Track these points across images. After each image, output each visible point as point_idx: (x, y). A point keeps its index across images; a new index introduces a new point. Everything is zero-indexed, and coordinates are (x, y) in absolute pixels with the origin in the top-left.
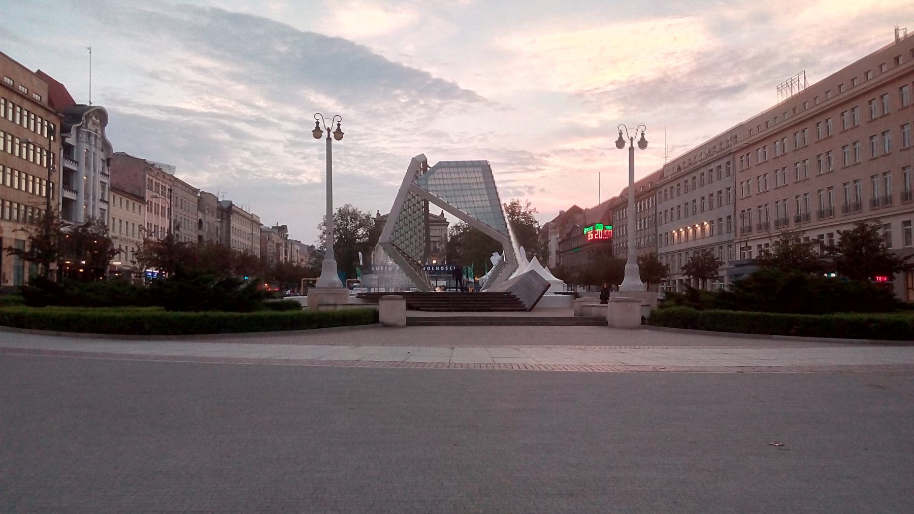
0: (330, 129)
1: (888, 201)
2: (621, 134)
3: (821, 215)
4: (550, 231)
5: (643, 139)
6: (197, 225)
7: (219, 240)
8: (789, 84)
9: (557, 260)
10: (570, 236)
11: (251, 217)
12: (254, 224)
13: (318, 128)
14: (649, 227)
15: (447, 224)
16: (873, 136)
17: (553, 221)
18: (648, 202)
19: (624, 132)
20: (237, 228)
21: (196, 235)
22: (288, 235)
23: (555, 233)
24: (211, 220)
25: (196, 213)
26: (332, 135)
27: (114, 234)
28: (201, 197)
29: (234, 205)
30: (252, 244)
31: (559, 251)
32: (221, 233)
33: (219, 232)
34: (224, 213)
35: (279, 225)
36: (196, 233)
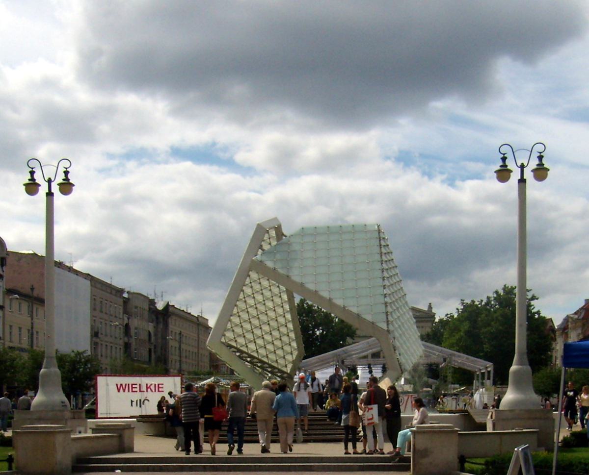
2: (504, 159)
4: (570, 326)
5: (541, 165)
6: (122, 330)
7: (152, 347)
17: (576, 313)
19: (509, 156)
23: (575, 328)
25: (121, 317)
27: (11, 345)
28: (128, 299)
30: (198, 350)
33: (153, 339)
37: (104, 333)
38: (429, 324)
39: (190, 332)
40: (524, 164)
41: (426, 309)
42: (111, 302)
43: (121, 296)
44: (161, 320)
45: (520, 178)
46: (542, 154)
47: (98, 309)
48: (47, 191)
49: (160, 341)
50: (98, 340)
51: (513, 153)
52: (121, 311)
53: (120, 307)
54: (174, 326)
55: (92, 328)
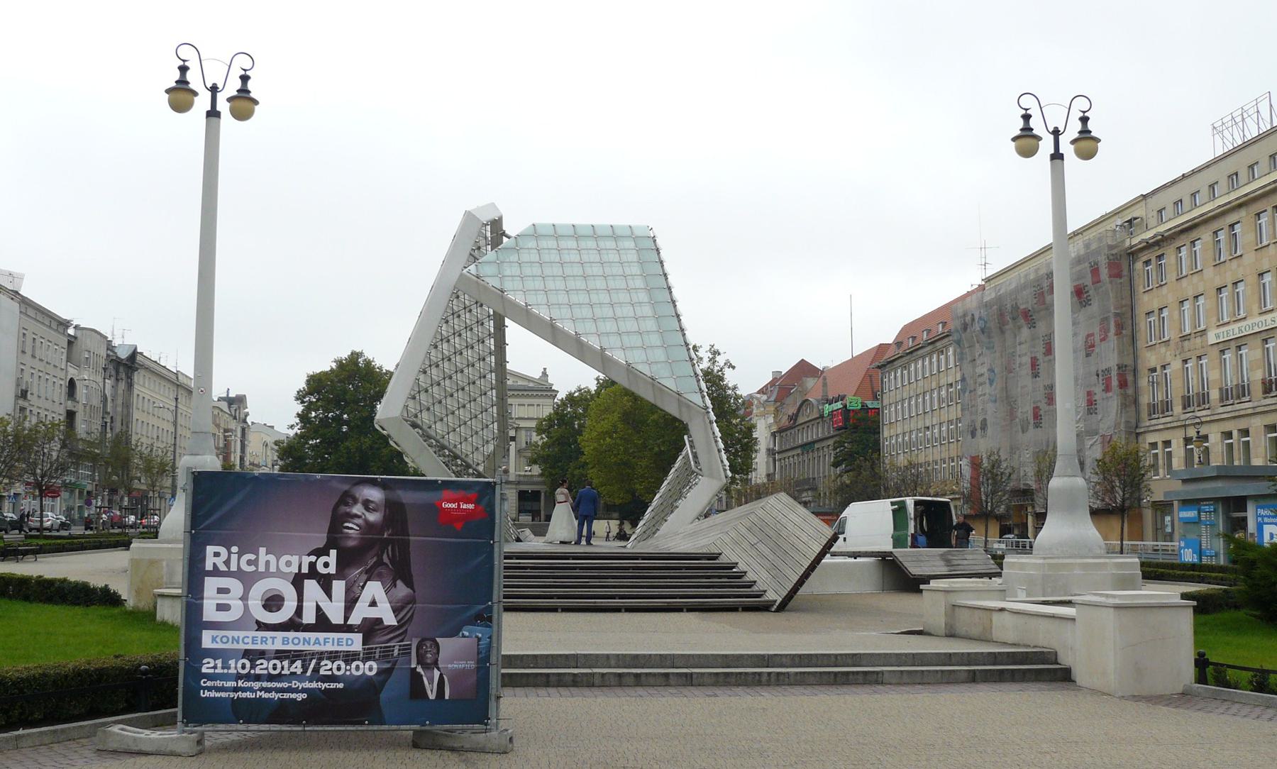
0: (221, 88)
1: (1242, 391)
3: (1225, 395)
5: (244, 91)
6: (65, 390)
8: (1239, 119)
9: (768, 468)
10: (796, 420)
11: (174, 377)
12: (181, 391)
13: (183, 81)
14: (940, 408)
15: (554, 394)
16: (1264, 273)
17: (761, 391)
18: (931, 363)
20: (147, 397)
21: (62, 410)
22: (247, 415)
23: (763, 415)
24: (91, 381)
26: (223, 106)
29: (141, 354)
31: (773, 450)
32: (115, 407)
33: (109, 404)
34: (121, 369)
35: (232, 395)
36: (62, 406)
37: (36, 393)
38: (549, 401)
39: (164, 397)
40: (1059, 129)
41: (536, 375)
42: (50, 342)
43: (64, 333)
44: (123, 376)
45: (1053, 152)
46: (1086, 114)
47: (29, 352)
48: (209, 109)
49: (119, 409)
50: (25, 404)
51: (1041, 108)
52: (64, 357)
53: (63, 350)
54: (143, 386)
55: (18, 382)
